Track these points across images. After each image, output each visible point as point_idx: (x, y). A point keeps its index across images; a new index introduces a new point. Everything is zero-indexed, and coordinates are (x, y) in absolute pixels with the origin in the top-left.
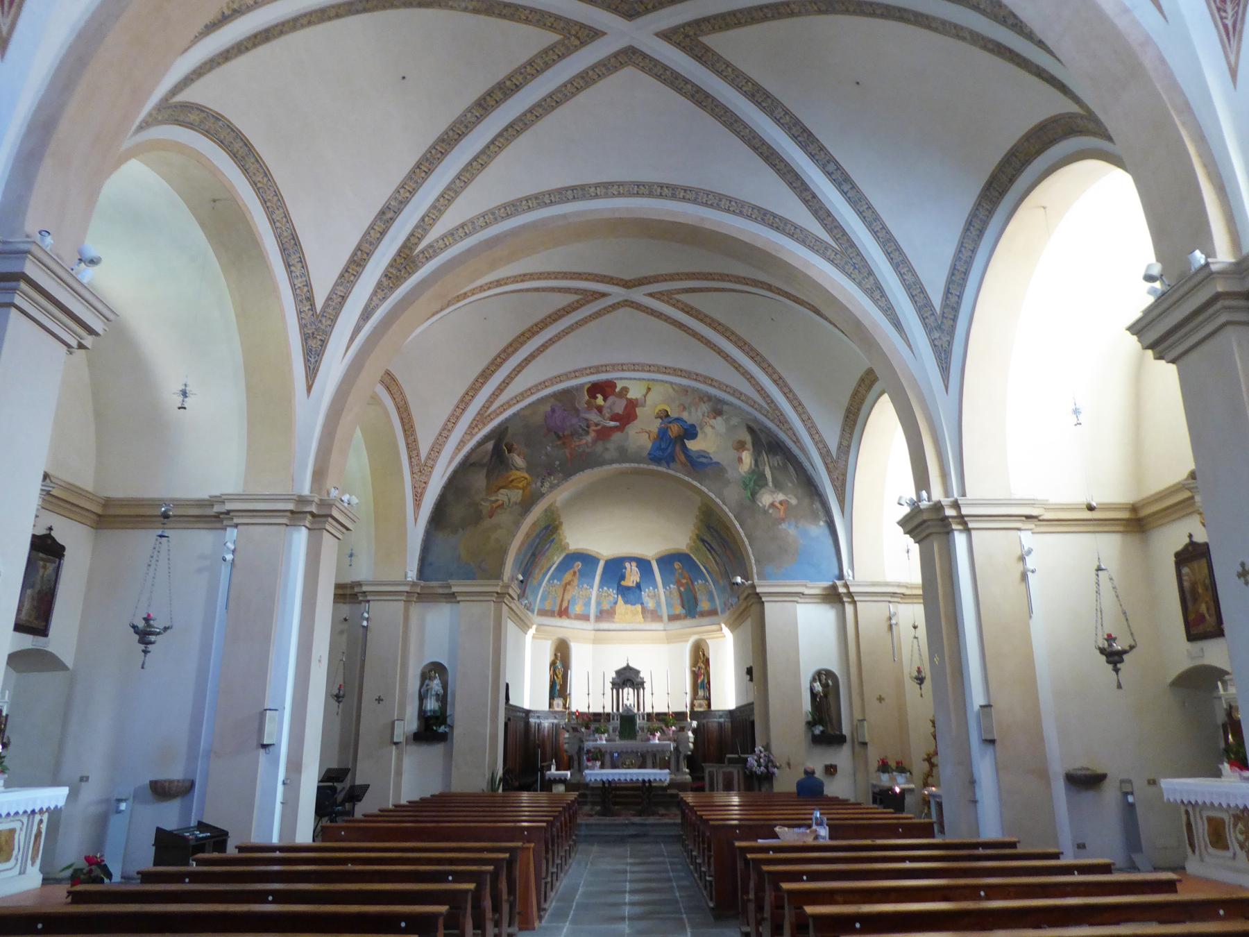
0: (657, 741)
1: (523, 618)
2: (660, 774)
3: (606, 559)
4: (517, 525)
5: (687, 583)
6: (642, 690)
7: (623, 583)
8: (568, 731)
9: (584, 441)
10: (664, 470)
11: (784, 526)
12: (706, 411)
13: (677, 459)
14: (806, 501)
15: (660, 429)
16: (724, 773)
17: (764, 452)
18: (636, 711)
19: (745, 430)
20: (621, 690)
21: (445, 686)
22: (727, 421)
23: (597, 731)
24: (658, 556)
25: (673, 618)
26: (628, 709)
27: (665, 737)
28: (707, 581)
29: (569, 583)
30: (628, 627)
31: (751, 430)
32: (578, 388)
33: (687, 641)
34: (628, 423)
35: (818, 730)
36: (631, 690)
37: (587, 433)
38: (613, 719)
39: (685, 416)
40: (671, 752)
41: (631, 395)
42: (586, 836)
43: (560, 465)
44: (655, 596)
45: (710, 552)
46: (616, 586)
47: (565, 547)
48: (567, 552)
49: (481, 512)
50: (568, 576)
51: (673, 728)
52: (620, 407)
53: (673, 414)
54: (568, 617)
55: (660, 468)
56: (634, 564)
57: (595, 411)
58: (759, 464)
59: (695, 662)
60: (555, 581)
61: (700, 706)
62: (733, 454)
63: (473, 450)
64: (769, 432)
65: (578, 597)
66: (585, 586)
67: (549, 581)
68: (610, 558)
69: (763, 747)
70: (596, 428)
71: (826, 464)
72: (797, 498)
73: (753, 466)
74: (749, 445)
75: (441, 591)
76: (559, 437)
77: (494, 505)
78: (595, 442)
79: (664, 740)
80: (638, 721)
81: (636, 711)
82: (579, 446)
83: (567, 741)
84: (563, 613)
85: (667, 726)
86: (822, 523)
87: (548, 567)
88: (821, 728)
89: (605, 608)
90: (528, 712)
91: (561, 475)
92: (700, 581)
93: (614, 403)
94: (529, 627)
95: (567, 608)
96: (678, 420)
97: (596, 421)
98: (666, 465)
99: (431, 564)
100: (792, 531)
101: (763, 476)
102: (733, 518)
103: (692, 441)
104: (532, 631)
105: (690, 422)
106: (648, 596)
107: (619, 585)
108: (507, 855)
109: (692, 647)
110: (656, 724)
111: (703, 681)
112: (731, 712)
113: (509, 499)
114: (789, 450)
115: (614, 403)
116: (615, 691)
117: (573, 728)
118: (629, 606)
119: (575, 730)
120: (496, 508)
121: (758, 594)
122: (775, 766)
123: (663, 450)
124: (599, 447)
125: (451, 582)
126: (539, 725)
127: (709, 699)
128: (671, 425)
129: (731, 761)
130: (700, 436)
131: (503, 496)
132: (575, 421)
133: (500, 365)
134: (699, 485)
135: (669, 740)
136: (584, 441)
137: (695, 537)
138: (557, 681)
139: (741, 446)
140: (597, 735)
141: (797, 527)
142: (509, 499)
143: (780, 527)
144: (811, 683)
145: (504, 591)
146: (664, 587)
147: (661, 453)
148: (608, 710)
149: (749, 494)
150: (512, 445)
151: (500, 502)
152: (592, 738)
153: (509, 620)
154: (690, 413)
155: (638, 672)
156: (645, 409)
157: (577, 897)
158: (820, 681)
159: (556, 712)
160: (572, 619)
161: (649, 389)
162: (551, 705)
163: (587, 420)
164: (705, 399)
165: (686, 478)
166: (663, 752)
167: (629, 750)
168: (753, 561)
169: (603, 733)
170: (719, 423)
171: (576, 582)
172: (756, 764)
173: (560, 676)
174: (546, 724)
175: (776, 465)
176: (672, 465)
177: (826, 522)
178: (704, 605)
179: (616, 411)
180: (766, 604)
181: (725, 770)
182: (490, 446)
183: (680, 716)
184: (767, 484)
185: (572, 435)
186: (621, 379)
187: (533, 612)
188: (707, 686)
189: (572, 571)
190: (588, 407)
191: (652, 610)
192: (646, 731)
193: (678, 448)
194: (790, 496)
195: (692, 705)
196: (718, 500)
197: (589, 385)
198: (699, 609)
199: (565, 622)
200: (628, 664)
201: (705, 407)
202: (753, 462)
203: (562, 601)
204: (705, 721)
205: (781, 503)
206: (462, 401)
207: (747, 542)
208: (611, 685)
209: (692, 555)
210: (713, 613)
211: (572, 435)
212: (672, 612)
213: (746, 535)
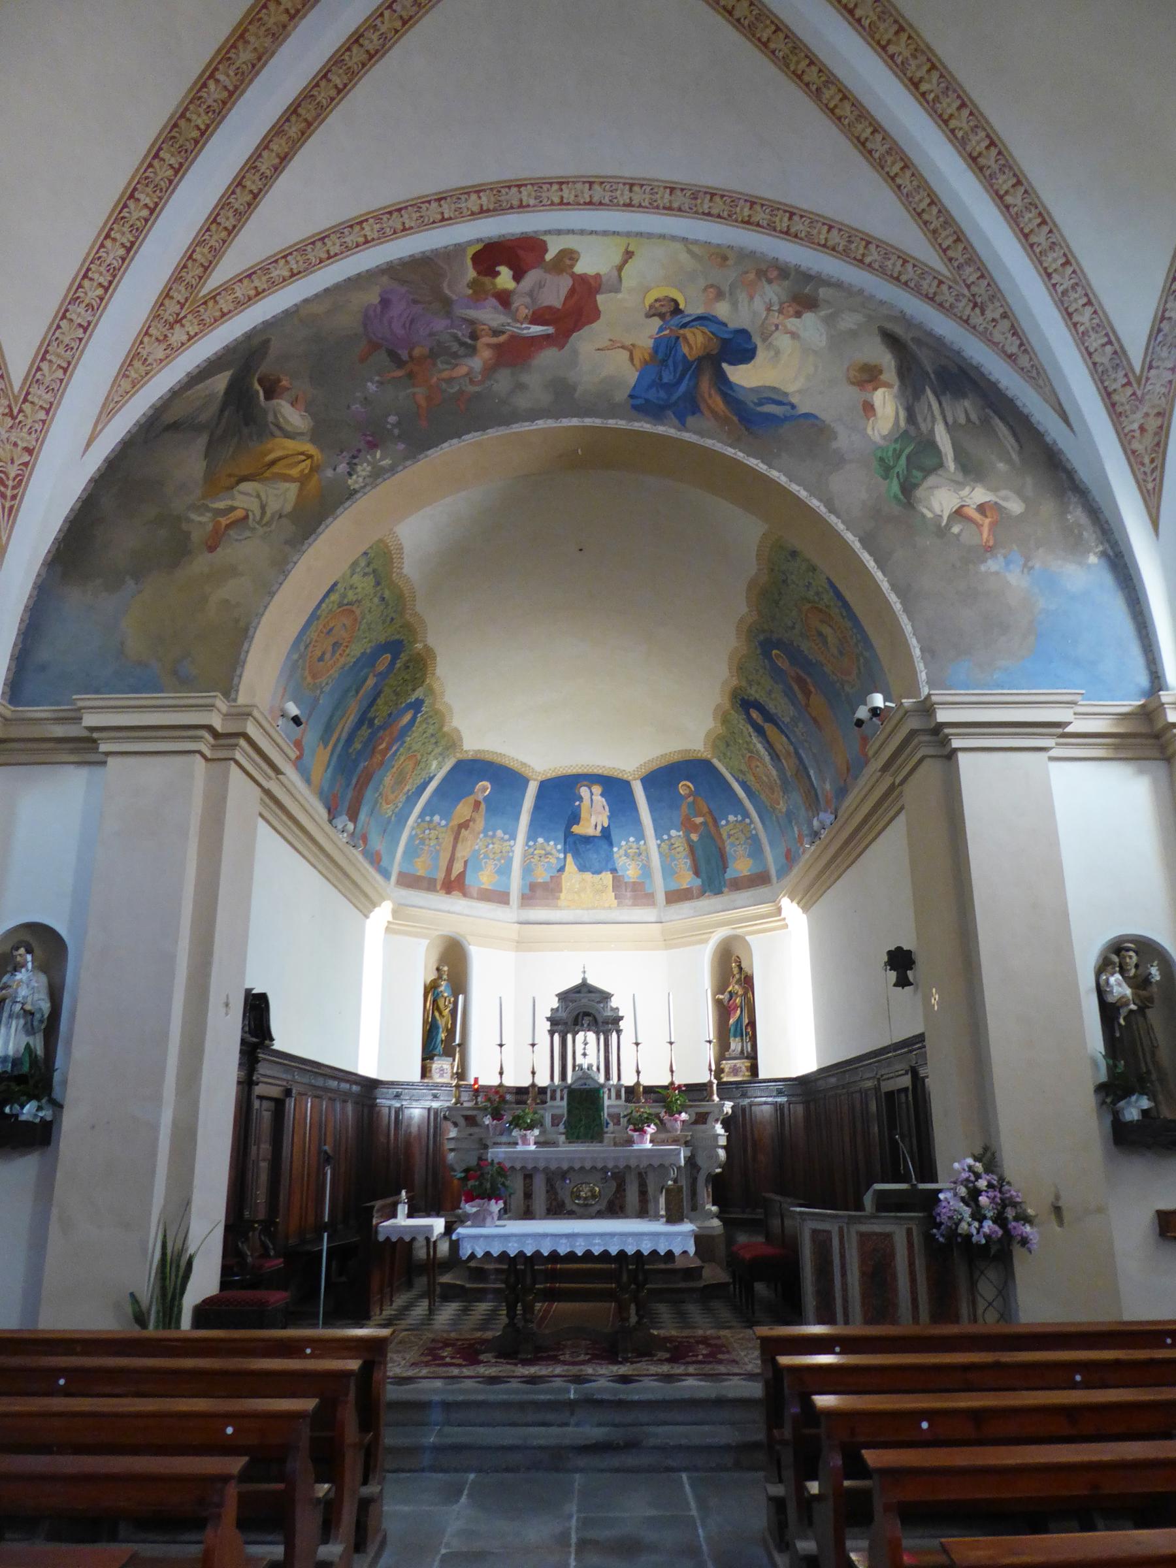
0: (649, 1146)
1: (360, 881)
2: (667, 1235)
3: (540, 778)
4: (282, 566)
5: (705, 824)
6: (614, 1035)
7: (576, 829)
8: (456, 1124)
9: (463, 370)
10: (672, 432)
11: (992, 565)
12: (775, 299)
13: (703, 407)
14: (1048, 507)
15: (658, 342)
16: (864, 1237)
17: (929, 392)
18: (602, 1080)
19: (878, 339)
20: (569, 1037)
21: (55, 994)
22: (829, 321)
23: (517, 1122)
24: (644, 772)
25: (675, 897)
26: (584, 1075)
27: (663, 1136)
28: (746, 815)
29: (465, 825)
30: (586, 915)
31: (892, 340)
32: (452, 254)
33: (706, 941)
34: (577, 327)
35: (1134, 1109)
36: (591, 1036)
37: (472, 350)
38: (553, 1098)
39: (722, 310)
40: (679, 1168)
41: (583, 267)
42: (437, 1449)
43: (398, 424)
44: (640, 855)
45: (760, 731)
46: (561, 835)
47: (452, 742)
48: (459, 756)
49: (187, 535)
50: (463, 810)
51: (684, 1116)
52: (555, 293)
53: (693, 306)
54: (465, 894)
55: (661, 429)
56: (597, 789)
57: (493, 301)
58: (920, 419)
59: (721, 985)
60: (437, 818)
61: (735, 1071)
62: (851, 394)
63: (175, 394)
64: (938, 345)
65: (486, 856)
66: (499, 833)
67: (422, 815)
68: (549, 776)
69: (976, 1159)
70: (495, 340)
71: (1108, 396)
72: (1025, 499)
73: (902, 423)
74: (890, 374)
75: (59, 731)
76: (399, 362)
77: (224, 521)
78: (490, 370)
79: (663, 1142)
80: (607, 1102)
81: (602, 1080)
82: (450, 380)
83: (451, 1145)
84: (454, 884)
85: (671, 1113)
86: (1093, 559)
87: (419, 781)
88: (1145, 1103)
89: (540, 880)
90: (371, 1085)
91: (401, 446)
92: (731, 818)
93: (541, 285)
94: (374, 905)
95: (462, 876)
96: (701, 319)
97: (494, 324)
98: (676, 422)
99: (43, 668)
100: (1016, 578)
101: (930, 445)
102: (857, 546)
103: (742, 367)
104: (382, 913)
105: (733, 325)
106: (627, 855)
107: (568, 834)
108: (308, 1404)
109: (715, 952)
110: (646, 1108)
111: (740, 1019)
112: (803, 1082)
113: (263, 508)
114: (994, 386)
115: (541, 285)
116: (556, 1037)
117: (467, 1118)
118: (588, 876)
119: (471, 1121)
120: (228, 526)
121: (938, 729)
122: (1027, 1219)
123: (670, 387)
124: (503, 381)
125: (83, 700)
126: (399, 1111)
127: (753, 1057)
128: (687, 332)
129: (886, 1203)
130: (761, 354)
131: (245, 498)
132: (440, 324)
133: (220, 111)
134: (762, 467)
135: (675, 1141)
136: (463, 370)
137: (727, 705)
138: (441, 1023)
139: (869, 376)
140: (515, 1133)
141: (1027, 567)
142: (263, 508)
143: (983, 568)
144: (1099, 972)
145: (232, 728)
146: (658, 836)
147: (662, 394)
148: (543, 1081)
149: (895, 487)
150: (279, 380)
151: (239, 514)
152: (504, 1139)
153: (261, 824)
154: (734, 304)
155: (606, 997)
156: (620, 296)
157: (559, 1266)
158: (1122, 971)
159: (437, 1086)
160: (472, 898)
161: (629, 255)
162: (425, 1072)
163: (472, 322)
164: (773, 274)
165: (730, 451)
166: (662, 1169)
167: (588, 1165)
168: (917, 652)
169: (530, 1127)
170: (810, 326)
171: (480, 824)
172: (967, 1211)
173: (446, 1012)
174: (416, 1112)
175: (962, 420)
176: (690, 420)
177: (1104, 554)
178: (741, 866)
179: (546, 303)
180: (962, 757)
181: (864, 1228)
182: (220, 382)
183: (697, 1091)
184: (941, 465)
185: (433, 355)
186: (559, 232)
187: (386, 874)
188: (749, 1030)
189: (471, 800)
190: (475, 292)
191: (634, 883)
192: (624, 1121)
193: (705, 384)
194: (1003, 493)
195: (719, 1072)
196: (815, 503)
197: (479, 247)
198: (730, 874)
199: (456, 904)
200: (584, 980)
201: (772, 293)
202: (902, 415)
203: (452, 860)
204: (746, 1102)
205: (982, 508)
206: (119, 214)
207: (897, 606)
208: (548, 1025)
209: (715, 762)
210: (760, 879)
211: (433, 355)
212: (674, 886)
213: (894, 587)
